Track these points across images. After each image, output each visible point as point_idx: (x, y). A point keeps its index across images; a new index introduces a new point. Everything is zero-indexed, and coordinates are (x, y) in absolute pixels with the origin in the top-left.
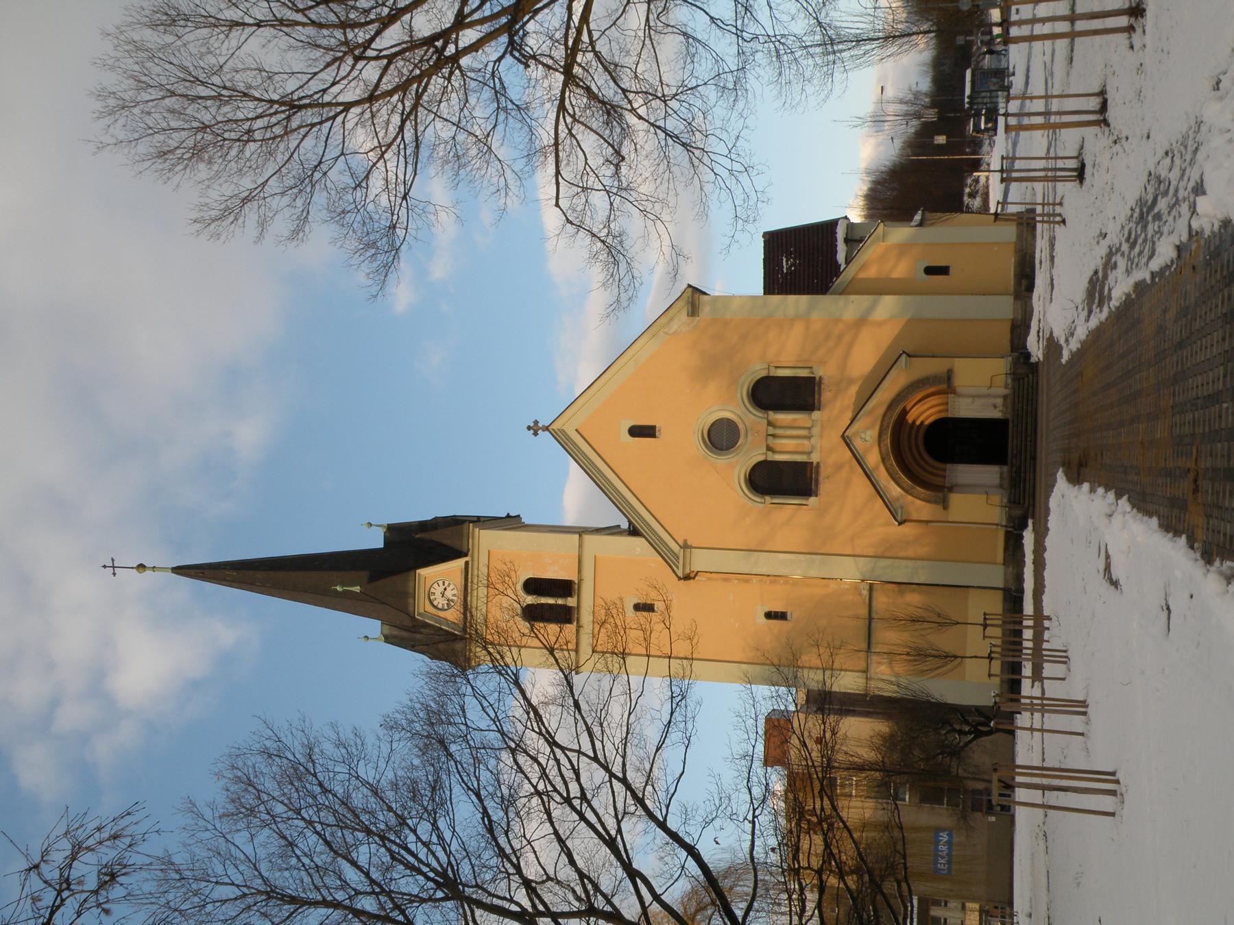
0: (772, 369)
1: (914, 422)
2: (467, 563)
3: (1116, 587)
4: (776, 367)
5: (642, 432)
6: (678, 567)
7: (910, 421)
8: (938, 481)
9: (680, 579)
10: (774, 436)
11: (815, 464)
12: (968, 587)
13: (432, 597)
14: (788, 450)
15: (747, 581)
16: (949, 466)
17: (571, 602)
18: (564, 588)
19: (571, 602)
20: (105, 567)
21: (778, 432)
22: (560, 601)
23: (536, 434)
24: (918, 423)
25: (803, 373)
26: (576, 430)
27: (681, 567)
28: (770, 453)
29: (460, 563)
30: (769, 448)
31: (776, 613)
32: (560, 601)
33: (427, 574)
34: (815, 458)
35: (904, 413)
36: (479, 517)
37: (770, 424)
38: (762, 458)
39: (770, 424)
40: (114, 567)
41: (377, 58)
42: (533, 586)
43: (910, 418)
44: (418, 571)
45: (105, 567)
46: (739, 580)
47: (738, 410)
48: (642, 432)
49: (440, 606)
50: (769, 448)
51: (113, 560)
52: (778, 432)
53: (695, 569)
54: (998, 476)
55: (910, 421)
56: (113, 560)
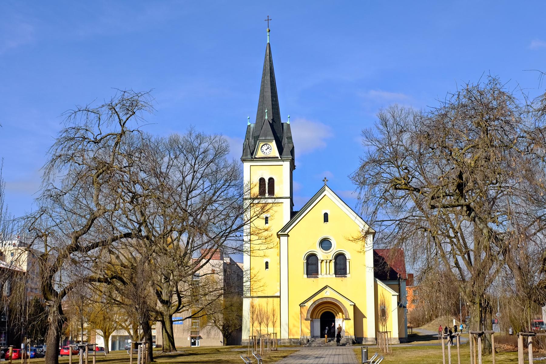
0: (349, 261)
1: (339, 314)
2: (278, 158)
3: (266, 269)
4: (349, 262)
5: (326, 218)
6: (281, 232)
7: (339, 313)
8: (314, 316)
9: (277, 233)
10: (326, 262)
11: (318, 276)
12: (280, 327)
13: (265, 145)
14: (322, 267)
15: (278, 255)
16: (320, 319)
17: (267, 195)
18: (272, 191)
19: (267, 195)
20: (268, 16)
21: (328, 263)
22: (267, 191)
23: (324, 181)
24: (338, 315)
25: (348, 272)
26: (325, 195)
27: (282, 233)
28: (321, 261)
29: (277, 155)
30: (322, 261)
31: (268, 265)
32: (267, 191)
33: (273, 145)
34: (319, 276)
35: (343, 314)
36: (294, 159)
37: (331, 261)
38: (319, 259)
39: (331, 261)
40: (268, 20)
41: (122, 299)
42: (271, 180)
43: (340, 314)
44: (274, 140)
45: (268, 16)
46: (278, 252)
47: (335, 249)
48: (326, 218)
49: (262, 148)
50: (322, 261)
51: (271, 20)
52: (328, 263)
53: (281, 238)
54: (317, 335)
55: (339, 313)
56: (271, 20)
